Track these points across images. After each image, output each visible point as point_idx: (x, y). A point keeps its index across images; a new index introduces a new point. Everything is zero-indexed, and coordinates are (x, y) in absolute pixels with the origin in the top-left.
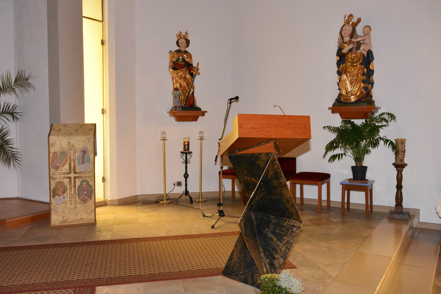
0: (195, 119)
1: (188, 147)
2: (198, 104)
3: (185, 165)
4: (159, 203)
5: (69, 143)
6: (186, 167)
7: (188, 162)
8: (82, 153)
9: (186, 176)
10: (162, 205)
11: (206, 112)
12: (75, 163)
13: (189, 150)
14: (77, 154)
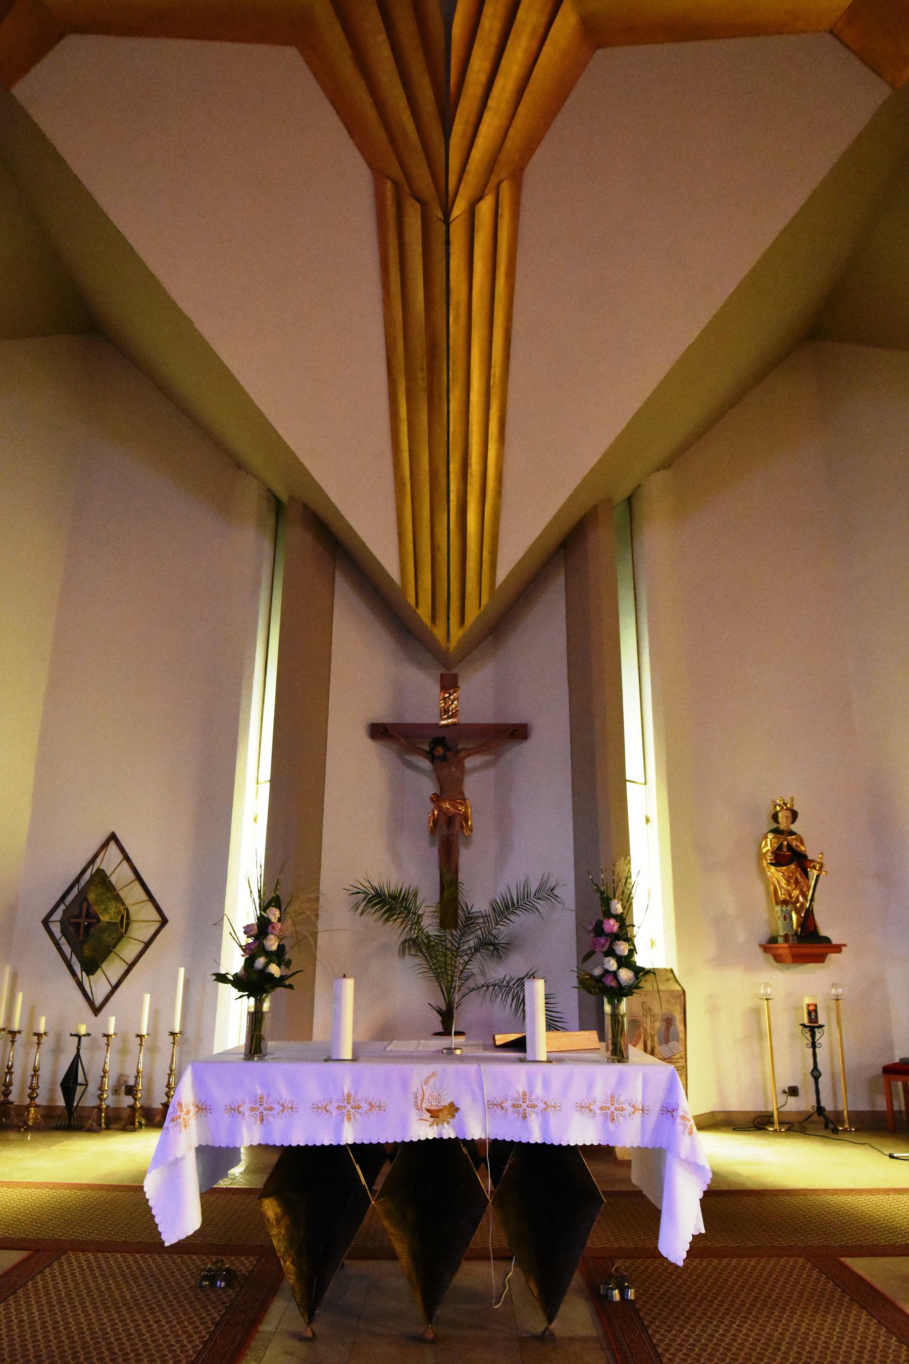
0: (820, 958)
1: (816, 1016)
2: (823, 931)
3: (811, 1050)
4: (765, 1129)
5: (644, 1003)
6: (815, 1055)
7: (817, 1045)
8: (664, 1023)
9: (816, 1074)
10: (771, 1133)
11: (845, 945)
12: (653, 1041)
13: (817, 1022)
14: (657, 1024)
